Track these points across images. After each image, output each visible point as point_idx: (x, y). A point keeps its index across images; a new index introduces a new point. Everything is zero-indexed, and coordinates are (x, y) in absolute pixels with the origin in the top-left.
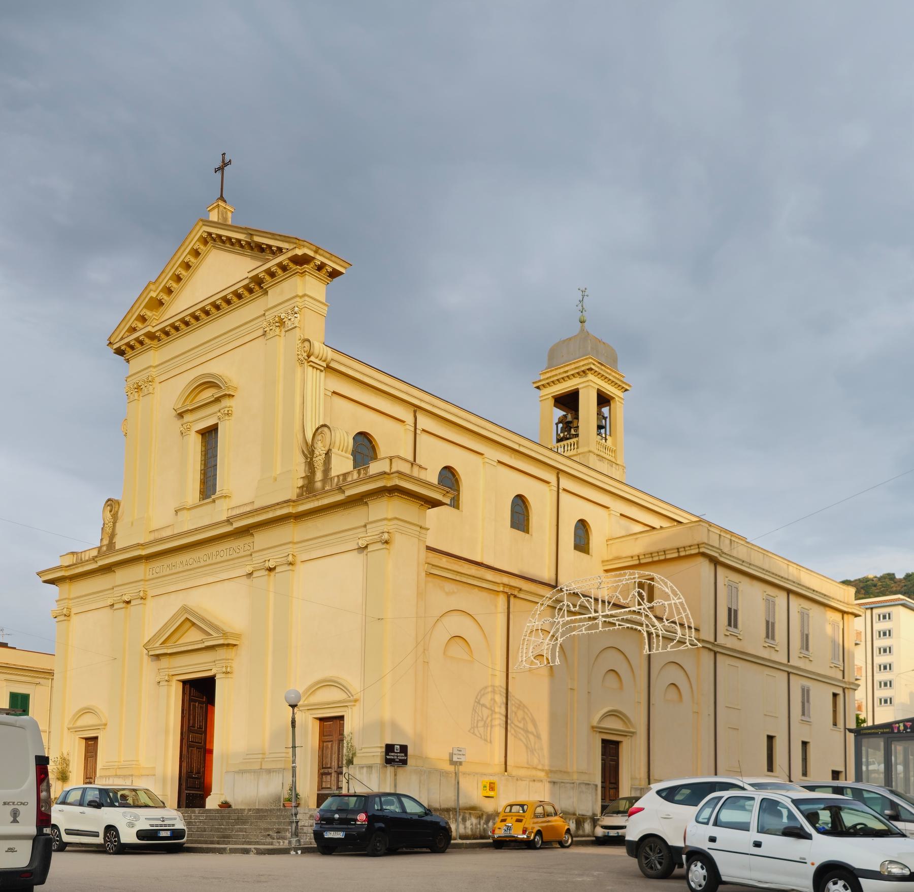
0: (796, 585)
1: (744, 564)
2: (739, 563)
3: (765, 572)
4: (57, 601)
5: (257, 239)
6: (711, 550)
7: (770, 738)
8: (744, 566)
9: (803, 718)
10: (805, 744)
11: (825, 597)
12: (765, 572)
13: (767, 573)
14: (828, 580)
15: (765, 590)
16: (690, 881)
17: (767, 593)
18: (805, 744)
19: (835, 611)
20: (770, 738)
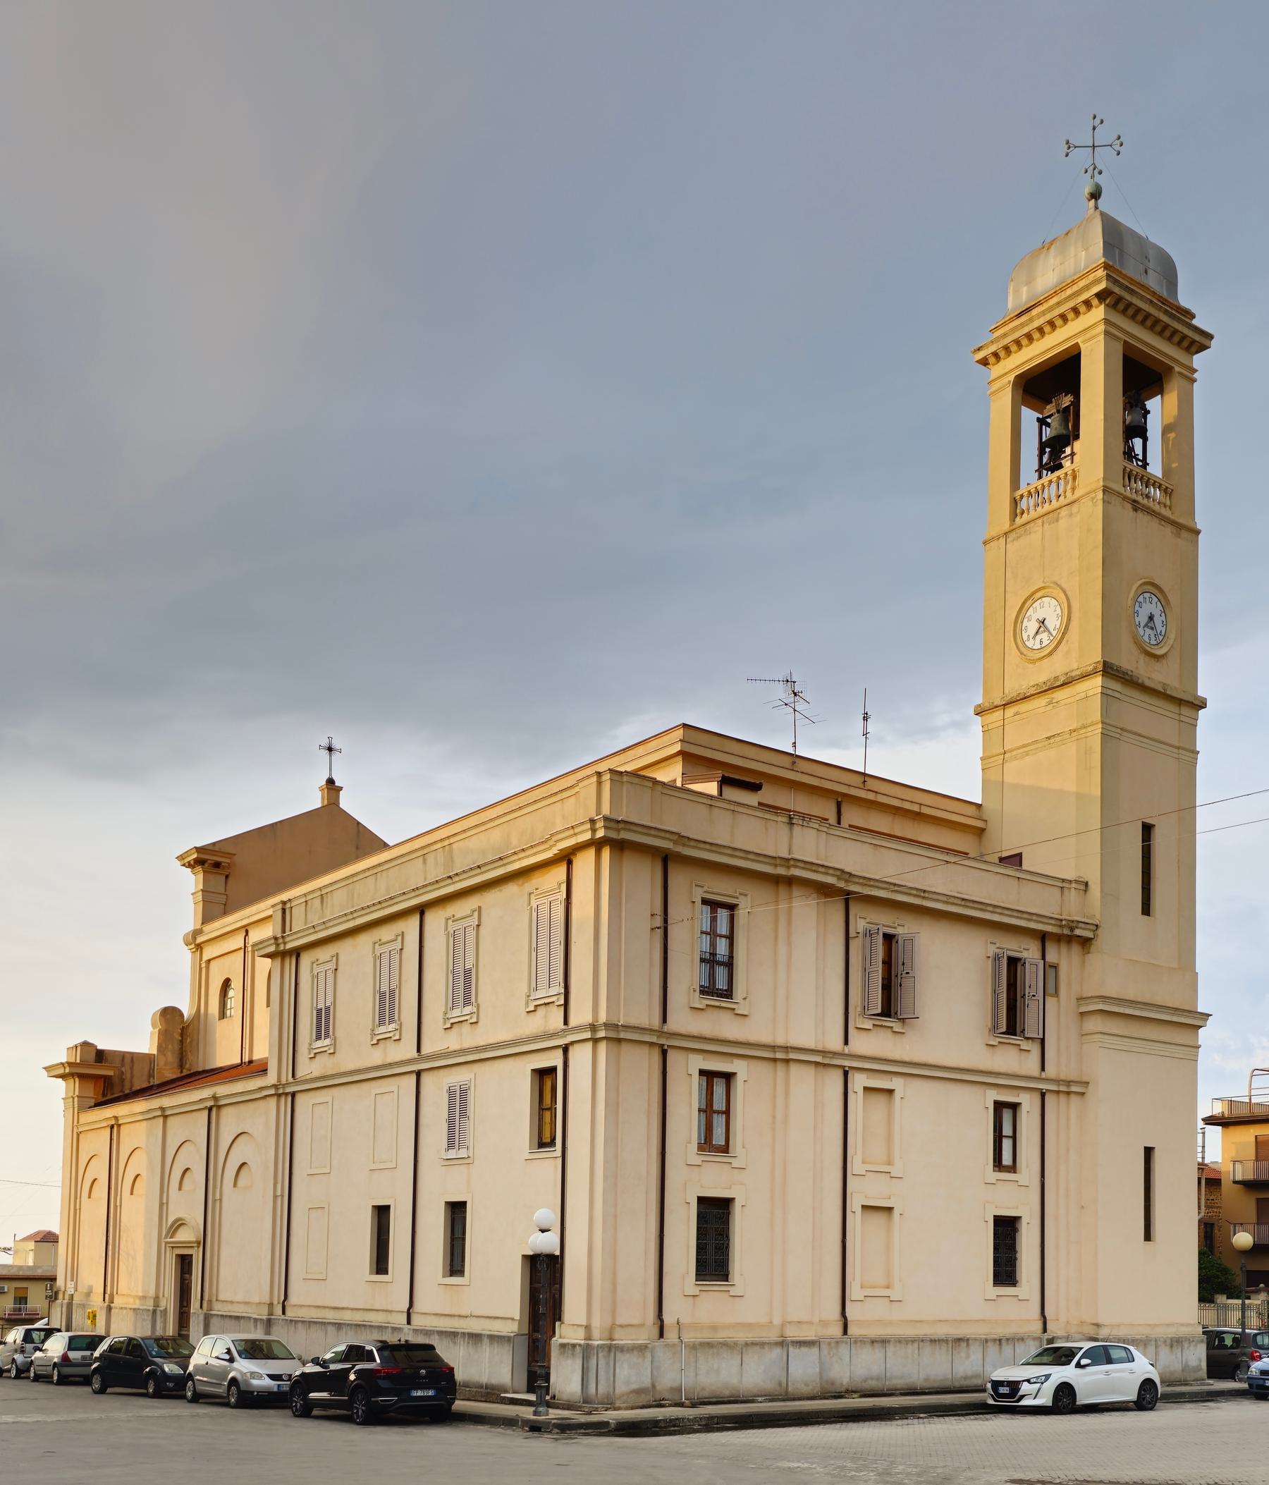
0: (413, 894)
1: (317, 929)
2: (310, 934)
3: (350, 917)
4: (63, 1099)
5: (1078, 932)
6: (264, 948)
7: (382, 1213)
8: (320, 931)
9: (452, 1154)
10: (457, 1211)
11: (483, 869)
12: (350, 917)
13: (355, 915)
14: (469, 834)
15: (994, 941)
16: (182, 1075)
17: (998, 945)
18: (457, 1211)
19: (544, 870)
20: (382, 1213)
